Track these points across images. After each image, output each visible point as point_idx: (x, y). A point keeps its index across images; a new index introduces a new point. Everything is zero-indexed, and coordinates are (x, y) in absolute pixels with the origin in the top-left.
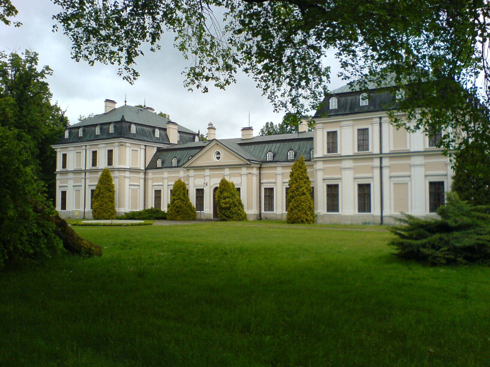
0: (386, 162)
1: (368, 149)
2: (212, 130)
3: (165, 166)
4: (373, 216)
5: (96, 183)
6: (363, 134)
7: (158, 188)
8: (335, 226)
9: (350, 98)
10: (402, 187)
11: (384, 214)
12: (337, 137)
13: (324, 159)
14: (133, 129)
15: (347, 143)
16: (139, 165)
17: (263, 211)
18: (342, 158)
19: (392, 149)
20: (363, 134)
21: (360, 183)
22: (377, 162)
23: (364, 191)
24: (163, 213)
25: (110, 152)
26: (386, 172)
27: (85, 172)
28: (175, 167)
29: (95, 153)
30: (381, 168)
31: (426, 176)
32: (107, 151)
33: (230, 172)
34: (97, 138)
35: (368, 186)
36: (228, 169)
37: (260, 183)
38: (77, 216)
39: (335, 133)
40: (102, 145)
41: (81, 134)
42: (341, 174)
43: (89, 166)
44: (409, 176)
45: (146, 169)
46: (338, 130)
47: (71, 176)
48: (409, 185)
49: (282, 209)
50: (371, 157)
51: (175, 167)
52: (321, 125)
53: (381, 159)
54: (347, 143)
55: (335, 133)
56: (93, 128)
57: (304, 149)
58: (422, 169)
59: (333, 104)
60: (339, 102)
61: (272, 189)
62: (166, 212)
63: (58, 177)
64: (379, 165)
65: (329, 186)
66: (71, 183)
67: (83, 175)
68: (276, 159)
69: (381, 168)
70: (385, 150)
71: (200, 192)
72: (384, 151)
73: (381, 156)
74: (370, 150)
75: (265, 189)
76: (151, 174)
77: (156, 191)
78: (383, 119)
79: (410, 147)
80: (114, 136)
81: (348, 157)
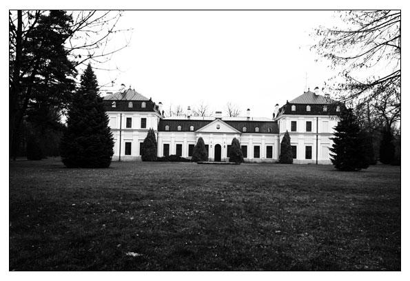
11: (318, 160)
15: (301, 126)
18: (132, 131)
43: (124, 126)
47: (135, 133)
54: (301, 126)
60: (146, 105)
71: (179, 147)
73: (121, 130)
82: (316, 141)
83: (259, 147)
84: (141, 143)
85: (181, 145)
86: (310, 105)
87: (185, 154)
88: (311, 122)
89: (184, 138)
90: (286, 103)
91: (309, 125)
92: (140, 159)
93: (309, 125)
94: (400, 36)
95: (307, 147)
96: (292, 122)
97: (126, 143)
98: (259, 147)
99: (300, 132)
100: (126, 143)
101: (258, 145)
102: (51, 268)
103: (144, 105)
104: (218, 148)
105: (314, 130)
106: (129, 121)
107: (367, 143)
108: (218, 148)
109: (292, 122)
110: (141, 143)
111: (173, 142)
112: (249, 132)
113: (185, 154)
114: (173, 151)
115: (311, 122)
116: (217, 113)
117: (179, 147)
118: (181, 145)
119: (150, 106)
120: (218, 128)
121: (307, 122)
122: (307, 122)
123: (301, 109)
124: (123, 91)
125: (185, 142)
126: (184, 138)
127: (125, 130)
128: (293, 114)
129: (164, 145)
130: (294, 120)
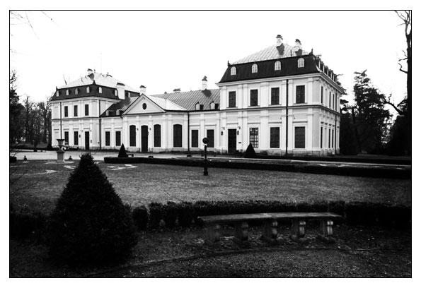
2: (143, 89)
7: (118, 130)
8: (277, 156)
14: (100, 91)
15: (264, 99)
17: (190, 147)
22: (284, 112)
25: (87, 107)
26: (290, 119)
27: (61, 120)
28: (213, 110)
29: (66, 108)
32: (270, 90)
35: (278, 129)
36: (311, 109)
37: (189, 126)
39: (303, 87)
41: (67, 94)
43: (63, 117)
45: (100, 116)
47: (240, 114)
51: (213, 110)
52: (246, 85)
54: (264, 99)
55: (303, 87)
59: (234, 71)
62: (237, 149)
63: (53, 123)
67: (284, 112)
72: (289, 105)
73: (287, 108)
75: (192, 131)
76: (103, 120)
77: (208, 131)
78: (289, 81)
81: (243, 110)
82: (98, 126)
83: (109, 132)
85: (213, 131)
86: (256, 63)
89: (201, 120)
90: (227, 67)
95: (272, 129)
96: (272, 89)
97: (106, 132)
98: (109, 132)
99: (261, 107)
100: (106, 132)
102: (13, 251)
103: (301, 63)
105: (282, 102)
107: (373, 137)
109: (272, 89)
111: (113, 128)
114: (242, 145)
116: (118, 84)
118: (213, 131)
119: (311, 64)
122: (230, 93)
123: (265, 69)
124: (279, 45)
125: (113, 128)
126: (201, 120)
127: (293, 108)
130: (254, 88)
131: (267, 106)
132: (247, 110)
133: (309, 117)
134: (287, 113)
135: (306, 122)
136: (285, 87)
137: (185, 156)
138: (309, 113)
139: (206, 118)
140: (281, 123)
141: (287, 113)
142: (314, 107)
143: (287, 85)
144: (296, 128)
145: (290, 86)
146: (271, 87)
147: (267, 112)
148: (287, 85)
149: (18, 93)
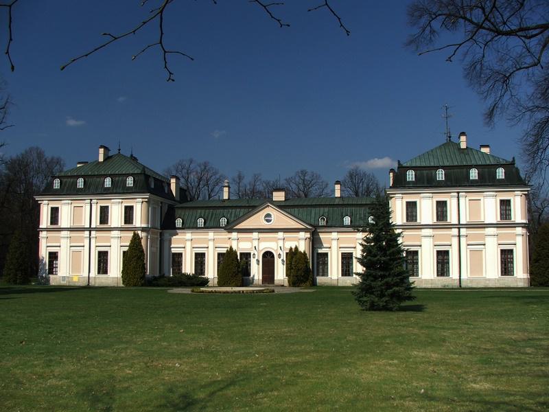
0: (463, 231)
1: (416, 220)
3: (187, 226)
4: (517, 279)
5: (128, 244)
6: (442, 206)
9: (425, 172)
10: (477, 257)
12: (416, 208)
13: (47, 230)
15: (427, 212)
16: (83, 222)
18: (111, 229)
19: (468, 220)
20: (442, 206)
21: (502, 248)
23: (443, 259)
24: (188, 277)
26: (93, 241)
27: (90, 229)
30: (459, 236)
31: (60, 247)
33: (498, 232)
34: (107, 192)
35: (447, 253)
38: (75, 282)
39: (415, 203)
40: (488, 193)
42: (110, 242)
43: (96, 223)
44: (355, 248)
46: (448, 200)
47: (64, 233)
48: (484, 252)
49: (338, 274)
50: (450, 227)
52: (464, 194)
53: (459, 228)
54: (427, 212)
56: (433, 172)
57: (358, 215)
58: (495, 239)
61: (203, 255)
63: (43, 234)
64: (88, 236)
65: (439, 253)
66: (65, 244)
67: (455, 231)
68: (329, 224)
69: (459, 236)
70: (93, 226)
71: (200, 259)
74: (418, 221)
77: (196, 254)
79: (451, 220)
80: (111, 191)
83: (106, 253)
84: (124, 252)
87: (211, 272)
88: (445, 203)
91: (441, 207)
92: (286, 284)
93: (441, 207)
94: (116, 38)
95: (439, 253)
97: (100, 253)
100: (100, 253)
101: (194, 255)
104: (268, 258)
105: (452, 218)
106: (104, 212)
108: (268, 258)
110: (124, 252)
112: (207, 228)
113: (211, 272)
115: (445, 203)
117: (200, 259)
120: (268, 215)
121: (438, 203)
122: (438, 203)
127: (97, 229)
128: (410, 188)
129: (197, 255)
130: (411, 199)
131: (495, 222)
132: (121, 229)
133: (112, 240)
134: (90, 235)
135: (110, 246)
136: (89, 207)
137: (403, 304)
138: (254, 238)
139: (239, 236)
140: (84, 246)
141: (90, 235)
142: (71, 230)
143: (458, 197)
144: (502, 251)
145: (462, 200)
146: (99, 205)
147: (495, 229)
148: (458, 197)
149: (158, 167)
